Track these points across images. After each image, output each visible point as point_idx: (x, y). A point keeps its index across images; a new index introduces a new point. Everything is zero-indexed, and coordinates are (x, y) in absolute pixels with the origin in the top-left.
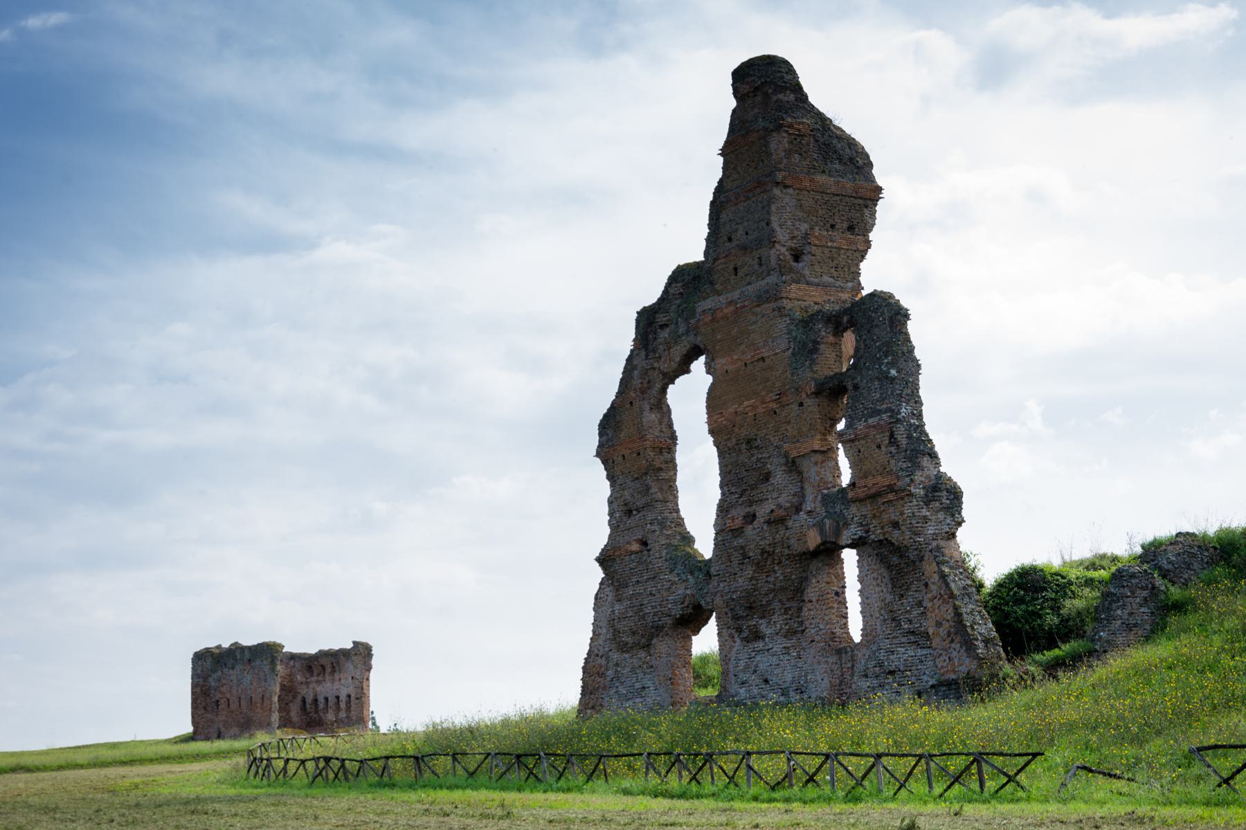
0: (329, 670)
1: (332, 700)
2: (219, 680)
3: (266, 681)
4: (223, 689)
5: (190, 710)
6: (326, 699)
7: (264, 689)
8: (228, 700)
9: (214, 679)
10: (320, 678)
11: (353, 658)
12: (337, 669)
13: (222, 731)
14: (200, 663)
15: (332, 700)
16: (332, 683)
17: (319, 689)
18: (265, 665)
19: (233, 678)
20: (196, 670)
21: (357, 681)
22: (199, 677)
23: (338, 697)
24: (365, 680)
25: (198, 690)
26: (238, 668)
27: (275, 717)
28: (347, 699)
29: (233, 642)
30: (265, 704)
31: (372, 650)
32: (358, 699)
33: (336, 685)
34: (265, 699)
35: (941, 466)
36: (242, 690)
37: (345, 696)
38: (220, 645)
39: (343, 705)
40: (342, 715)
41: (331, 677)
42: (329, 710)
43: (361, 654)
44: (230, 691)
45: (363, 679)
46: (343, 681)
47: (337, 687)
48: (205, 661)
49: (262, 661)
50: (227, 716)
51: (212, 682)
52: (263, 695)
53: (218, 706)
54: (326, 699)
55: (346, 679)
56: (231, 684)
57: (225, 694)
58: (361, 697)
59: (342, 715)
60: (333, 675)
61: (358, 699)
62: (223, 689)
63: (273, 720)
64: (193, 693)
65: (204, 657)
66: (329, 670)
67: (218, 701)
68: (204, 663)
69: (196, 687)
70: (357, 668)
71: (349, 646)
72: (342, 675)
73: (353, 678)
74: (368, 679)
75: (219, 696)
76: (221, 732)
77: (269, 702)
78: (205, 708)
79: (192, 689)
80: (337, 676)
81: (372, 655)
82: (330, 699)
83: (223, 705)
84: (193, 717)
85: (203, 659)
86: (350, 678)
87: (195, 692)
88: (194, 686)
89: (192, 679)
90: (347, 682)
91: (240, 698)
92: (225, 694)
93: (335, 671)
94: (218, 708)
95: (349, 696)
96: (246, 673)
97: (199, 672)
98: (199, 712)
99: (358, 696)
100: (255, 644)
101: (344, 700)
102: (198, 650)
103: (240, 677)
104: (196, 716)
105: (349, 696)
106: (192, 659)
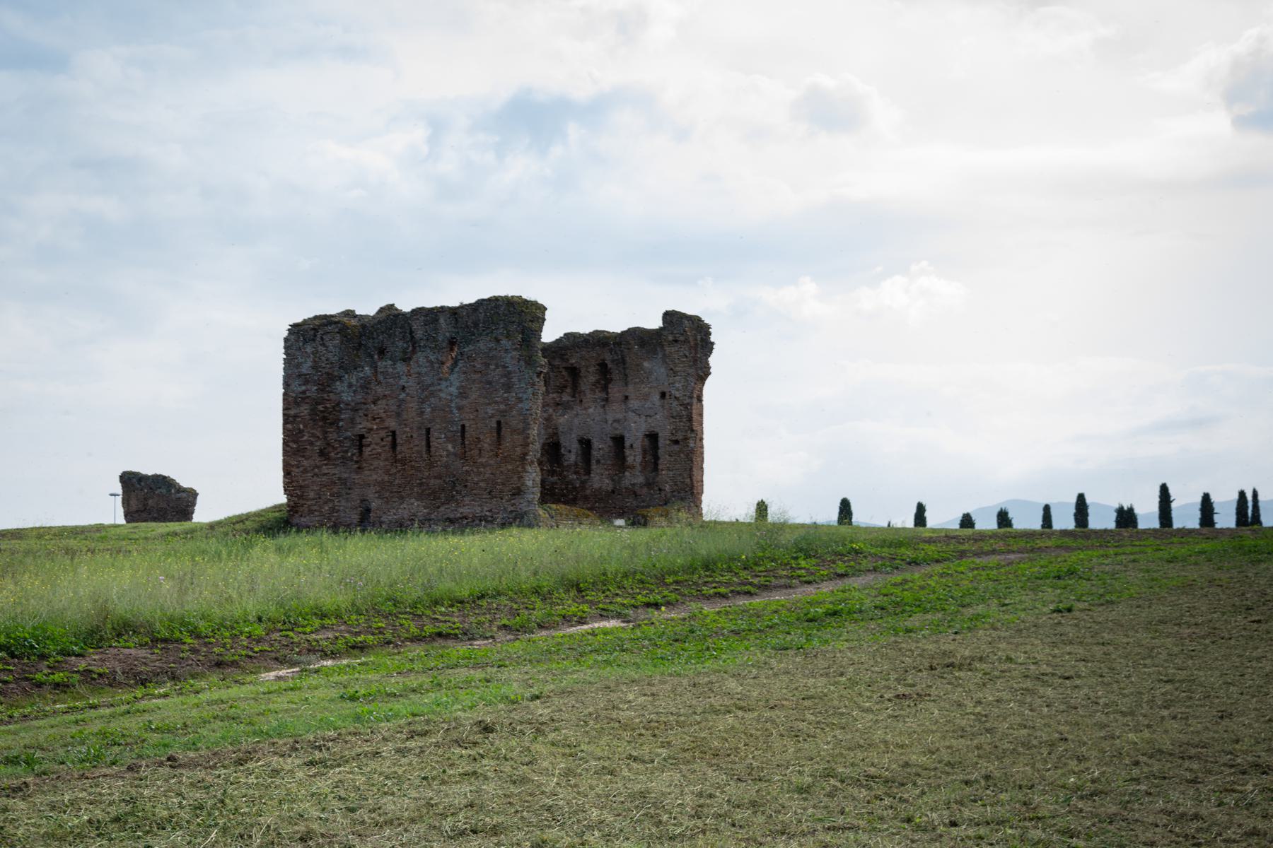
0: (589, 378)
1: (601, 447)
2: (366, 386)
3: (508, 387)
4: (379, 409)
5: (281, 458)
6: (586, 444)
7: (502, 407)
8: (394, 433)
9: (350, 386)
10: (566, 397)
11: (668, 349)
12: (616, 375)
13: (374, 505)
14: (309, 349)
15: (601, 447)
16: (604, 406)
17: (562, 420)
18: (506, 351)
19: (411, 383)
20: (299, 365)
21: (675, 403)
22: (306, 382)
23: (619, 441)
24: (695, 401)
25: (304, 410)
26: (420, 357)
27: (533, 477)
28: (647, 442)
29: (383, 304)
30: (507, 443)
31: (710, 334)
32: (676, 442)
33: (615, 412)
34: (505, 432)
35: (284, 359)
36: (433, 410)
37: (640, 435)
38: (393, 305)
39: (634, 457)
40: (634, 478)
41: (599, 395)
42: (594, 467)
43: (686, 341)
44: (398, 415)
45: (691, 397)
46: (634, 404)
47: (619, 416)
48: (323, 345)
49: (498, 341)
50: (387, 472)
51: (344, 392)
52: (499, 423)
53: (360, 447)
54: (586, 444)
55: (646, 397)
56: (403, 396)
57: (383, 421)
58: (686, 439)
59: (634, 478)
60: (605, 388)
61: (676, 442)
62: (379, 409)
63: (530, 483)
64: (287, 419)
65: (319, 335)
66: (589, 378)
67: (362, 437)
68: (321, 349)
69: (298, 404)
70: (675, 374)
71: (654, 322)
72: (631, 388)
73: (663, 395)
74: (700, 399)
75: (362, 425)
76: (368, 510)
77: (519, 439)
78: (322, 453)
79: (286, 409)
80: (615, 390)
81: (713, 344)
82: (596, 444)
83: (376, 443)
84: (287, 472)
85: (318, 339)
86: (656, 397)
87: (296, 416)
88: (290, 402)
89: (286, 384)
90: (648, 404)
91: (428, 431)
92: (383, 421)
93: (610, 381)
94: (361, 452)
95: (653, 437)
96: (445, 368)
97: (305, 369)
98: (305, 463)
99: (679, 436)
100: (471, 299)
101: (638, 445)
102: (299, 320)
103: (428, 380)
104: (295, 471)
105: (653, 437)
106: (286, 340)
